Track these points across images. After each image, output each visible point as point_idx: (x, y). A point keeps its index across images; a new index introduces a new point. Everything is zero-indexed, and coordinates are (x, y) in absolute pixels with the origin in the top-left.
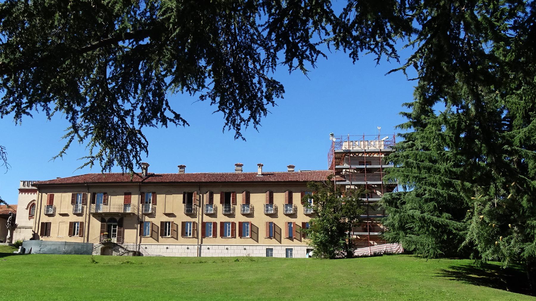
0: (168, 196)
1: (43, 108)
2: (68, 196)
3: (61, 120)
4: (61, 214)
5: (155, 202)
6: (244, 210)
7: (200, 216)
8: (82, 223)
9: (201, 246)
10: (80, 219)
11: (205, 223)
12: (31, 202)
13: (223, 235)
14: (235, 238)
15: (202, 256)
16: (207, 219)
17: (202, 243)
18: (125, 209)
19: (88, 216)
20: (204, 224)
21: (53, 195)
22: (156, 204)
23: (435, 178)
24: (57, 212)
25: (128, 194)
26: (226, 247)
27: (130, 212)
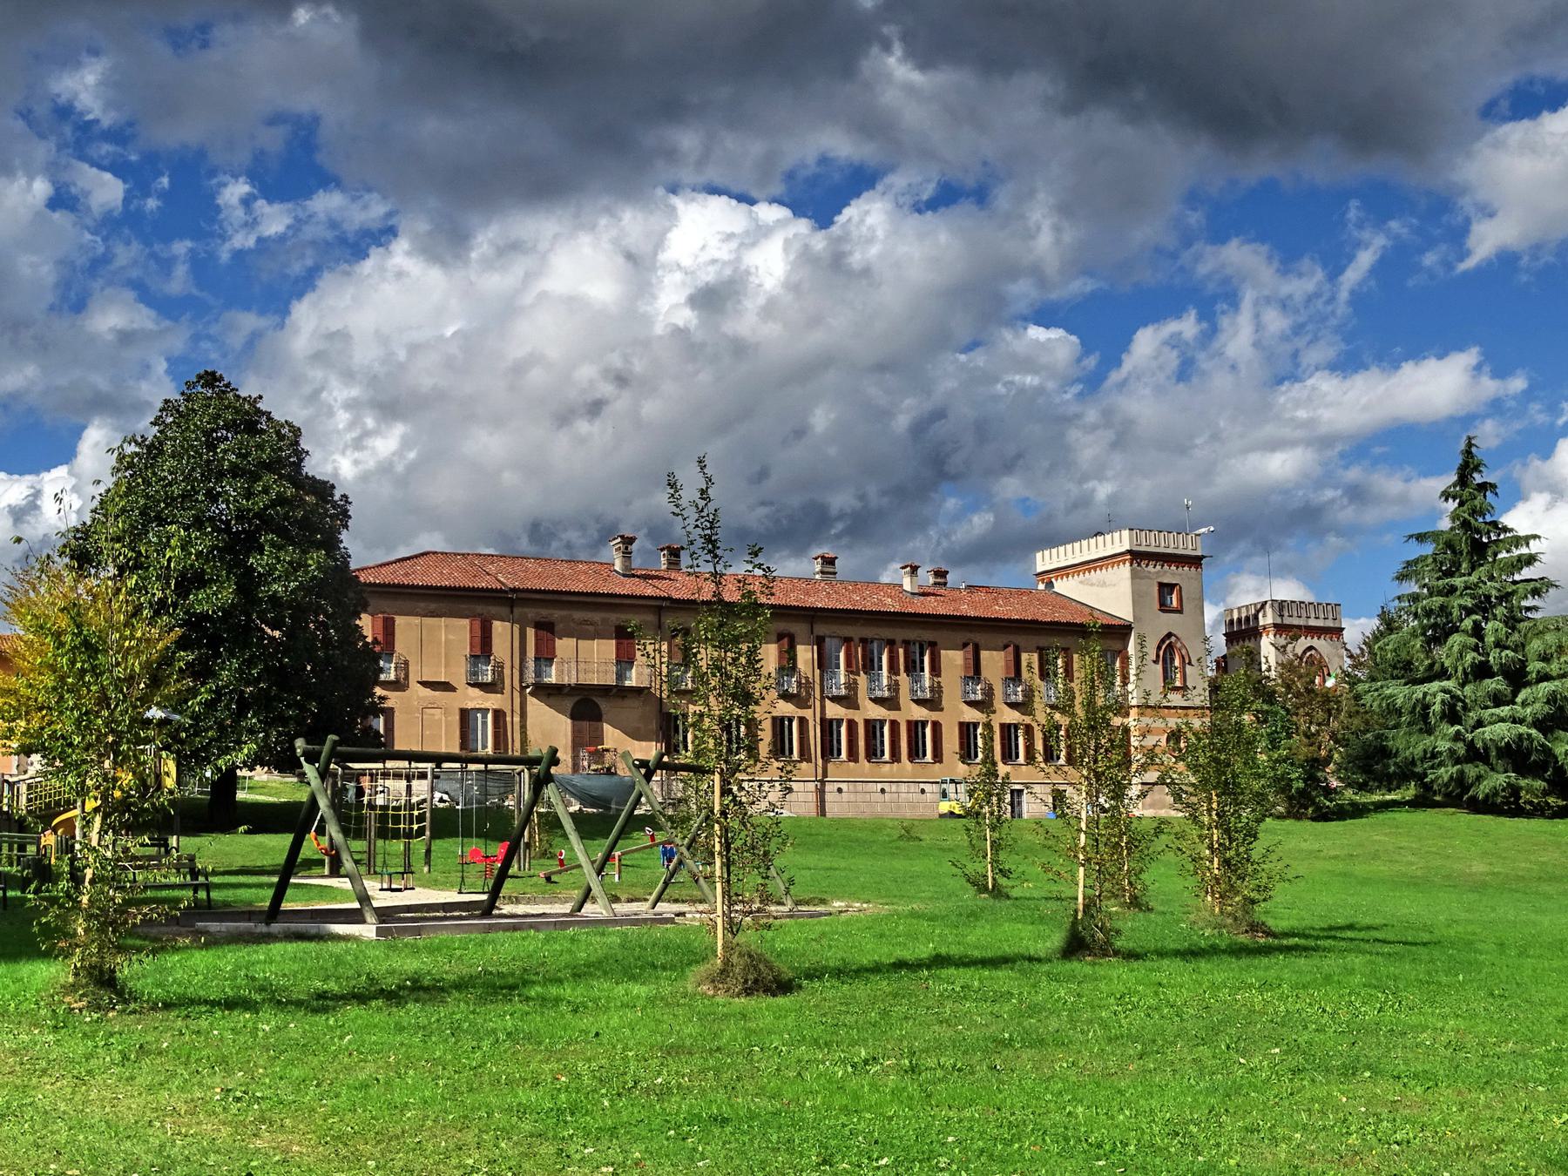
0: (583, 643)
1: (261, 406)
2: (455, 633)
3: (109, 482)
4: (425, 684)
5: (936, 670)
6: (475, 674)
7: (818, 704)
8: (499, 715)
9: (823, 782)
10: (492, 701)
11: (831, 721)
12: (1163, 641)
13: (873, 753)
14: (856, 761)
15: (832, 809)
16: (834, 711)
17: (825, 774)
18: (621, 676)
19: (517, 695)
20: (828, 726)
21: (393, 621)
22: (939, 675)
23: (1535, 645)
24: (413, 678)
25: (623, 636)
26: (880, 786)
27: (553, 680)
